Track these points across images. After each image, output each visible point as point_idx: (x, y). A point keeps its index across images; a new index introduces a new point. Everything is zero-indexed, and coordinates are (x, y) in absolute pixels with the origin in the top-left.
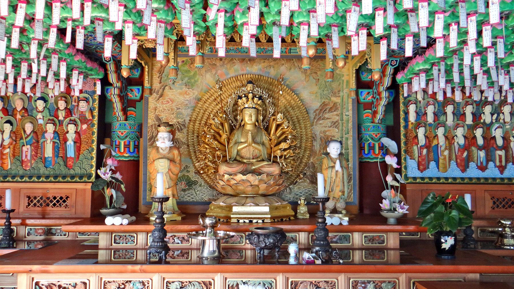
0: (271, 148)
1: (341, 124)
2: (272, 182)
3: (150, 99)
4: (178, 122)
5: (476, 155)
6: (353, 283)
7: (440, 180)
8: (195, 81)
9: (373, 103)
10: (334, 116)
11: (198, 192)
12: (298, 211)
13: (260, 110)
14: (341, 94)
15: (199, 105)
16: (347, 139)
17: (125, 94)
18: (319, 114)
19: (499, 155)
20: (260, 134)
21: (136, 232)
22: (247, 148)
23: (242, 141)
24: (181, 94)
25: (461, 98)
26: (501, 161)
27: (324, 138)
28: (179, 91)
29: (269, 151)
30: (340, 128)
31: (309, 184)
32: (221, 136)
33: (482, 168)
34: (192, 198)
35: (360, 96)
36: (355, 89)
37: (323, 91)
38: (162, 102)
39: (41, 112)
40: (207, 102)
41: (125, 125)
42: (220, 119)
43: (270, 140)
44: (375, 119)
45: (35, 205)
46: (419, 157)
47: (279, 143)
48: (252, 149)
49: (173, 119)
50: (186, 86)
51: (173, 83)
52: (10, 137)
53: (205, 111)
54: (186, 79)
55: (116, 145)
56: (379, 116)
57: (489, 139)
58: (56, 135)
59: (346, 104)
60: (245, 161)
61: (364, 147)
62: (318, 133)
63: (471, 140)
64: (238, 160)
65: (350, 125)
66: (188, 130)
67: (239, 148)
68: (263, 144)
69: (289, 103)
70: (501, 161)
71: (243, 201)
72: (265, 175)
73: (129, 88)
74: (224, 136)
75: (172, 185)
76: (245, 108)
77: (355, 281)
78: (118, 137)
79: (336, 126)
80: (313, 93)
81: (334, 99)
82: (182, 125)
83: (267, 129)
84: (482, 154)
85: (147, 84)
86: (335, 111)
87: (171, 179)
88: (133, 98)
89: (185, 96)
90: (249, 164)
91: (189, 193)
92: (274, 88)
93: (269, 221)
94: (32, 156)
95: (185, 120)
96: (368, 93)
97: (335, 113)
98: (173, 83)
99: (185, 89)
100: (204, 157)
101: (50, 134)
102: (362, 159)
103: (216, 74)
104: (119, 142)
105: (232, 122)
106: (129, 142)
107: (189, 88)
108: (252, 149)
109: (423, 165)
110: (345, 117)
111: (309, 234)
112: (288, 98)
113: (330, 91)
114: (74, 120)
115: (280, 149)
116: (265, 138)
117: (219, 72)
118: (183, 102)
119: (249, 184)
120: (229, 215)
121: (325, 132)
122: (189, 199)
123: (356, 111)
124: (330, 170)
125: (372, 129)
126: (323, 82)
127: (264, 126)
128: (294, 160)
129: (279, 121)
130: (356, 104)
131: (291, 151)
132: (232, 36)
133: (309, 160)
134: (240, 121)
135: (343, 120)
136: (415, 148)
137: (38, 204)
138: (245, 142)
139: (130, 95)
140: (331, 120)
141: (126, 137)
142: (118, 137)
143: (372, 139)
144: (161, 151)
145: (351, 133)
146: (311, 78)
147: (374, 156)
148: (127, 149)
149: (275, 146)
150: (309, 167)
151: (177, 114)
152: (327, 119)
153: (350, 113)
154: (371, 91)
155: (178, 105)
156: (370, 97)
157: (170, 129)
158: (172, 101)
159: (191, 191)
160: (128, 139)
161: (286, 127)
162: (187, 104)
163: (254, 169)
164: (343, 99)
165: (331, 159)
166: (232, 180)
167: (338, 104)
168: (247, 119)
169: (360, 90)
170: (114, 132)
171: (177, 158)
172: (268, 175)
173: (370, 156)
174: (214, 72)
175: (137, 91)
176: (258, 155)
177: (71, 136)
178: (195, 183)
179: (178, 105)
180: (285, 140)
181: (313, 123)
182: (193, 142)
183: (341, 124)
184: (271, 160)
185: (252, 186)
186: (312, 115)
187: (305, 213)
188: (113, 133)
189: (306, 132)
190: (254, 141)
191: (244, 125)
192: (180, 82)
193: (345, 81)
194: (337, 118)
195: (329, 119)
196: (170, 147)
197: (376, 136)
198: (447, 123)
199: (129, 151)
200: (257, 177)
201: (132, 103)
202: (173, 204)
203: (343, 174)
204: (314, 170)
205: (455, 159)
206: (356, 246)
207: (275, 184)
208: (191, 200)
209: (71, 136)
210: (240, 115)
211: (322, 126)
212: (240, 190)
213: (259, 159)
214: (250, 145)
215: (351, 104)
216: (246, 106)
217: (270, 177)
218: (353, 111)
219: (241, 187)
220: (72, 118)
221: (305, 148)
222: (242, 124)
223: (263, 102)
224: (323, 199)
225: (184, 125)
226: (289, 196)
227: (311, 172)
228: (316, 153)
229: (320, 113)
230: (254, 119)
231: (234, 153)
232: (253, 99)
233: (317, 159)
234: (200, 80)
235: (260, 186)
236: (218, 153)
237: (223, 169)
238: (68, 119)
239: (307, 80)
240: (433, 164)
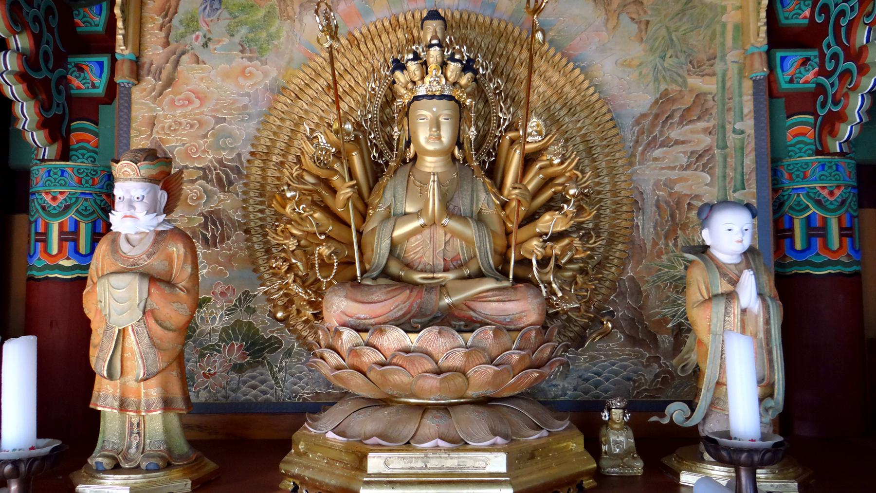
0: (508, 234)
1: (719, 158)
2: (516, 357)
3: (137, 94)
4: (220, 162)
8: (271, 37)
9: (821, 89)
10: (697, 135)
11: (282, 374)
12: (604, 448)
13: (469, 109)
14: (718, 67)
15: (279, 106)
17: (54, 77)
18: (650, 132)
20: (467, 187)
22: (427, 232)
23: (409, 209)
24: (226, 75)
27: (667, 203)
28: (224, 66)
29: (501, 242)
30: (718, 171)
31: (623, 345)
32: (334, 192)
34: (264, 393)
35: (779, 70)
36: (766, 48)
37: (663, 58)
38: (173, 101)
40: (305, 97)
41: (63, 172)
42: (333, 137)
43: (504, 205)
44: (829, 140)
47: (531, 218)
48: (440, 236)
49: (205, 151)
50: (242, 52)
51: (205, 45)
53: (296, 125)
54: (243, 31)
55: (37, 233)
56: (846, 131)
59: (736, 99)
60: (417, 277)
61: (791, 229)
62: (647, 188)
64: (394, 276)
65: (749, 161)
66: (245, 185)
67: (398, 233)
68: (480, 219)
69: (560, 93)
71: (409, 430)
72: (489, 331)
73: (73, 60)
74: (345, 192)
75: (161, 365)
76: (417, 98)
78: (43, 208)
80: (630, 66)
82: (231, 168)
83: (494, 173)
85: (122, 50)
86: (699, 119)
87: (154, 345)
88: (87, 91)
89: (241, 80)
90: (430, 288)
91: (253, 378)
92: (510, 46)
95: (239, 155)
96: (805, 62)
97: (701, 125)
98: (205, 45)
99: (240, 61)
100: (285, 267)
102: (784, 266)
104: (825, 220)
105: (381, 155)
106: (77, 224)
107: (250, 59)
108: (440, 236)
112: (555, 77)
115: (540, 235)
116: (486, 201)
118: (234, 102)
119: (430, 365)
120: (354, 486)
121: (669, 184)
122: (255, 396)
123: (765, 119)
124: (719, 307)
125: (818, 174)
126: (664, 32)
127: (479, 158)
128: (583, 271)
129: (533, 142)
130: (765, 96)
131: (577, 243)
132: (421, 59)
133: (620, 274)
134: (402, 145)
135: (725, 147)
138: (418, 215)
139: (76, 82)
140: (688, 148)
141: (67, 208)
142: (43, 208)
143: (819, 203)
144: (125, 247)
146: (625, 18)
147: (825, 257)
148: (68, 245)
149: (520, 226)
150: (622, 294)
151: (218, 136)
152: (677, 142)
153: (748, 125)
154: (813, 53)
155: (217, 111)
156: (810, 75)
157: (154, 172)
158: (202, 98)
159: (260, 369)
160: (72, 214)
161: (557, 161)
162: (245, 107)
163: (450, 307)
164: (724, 81)
165: (720, 267)
166: (368, 351)
167: (710, 97)
168: (423, 136)
169: (779, 54)
170: (34, 194)
171: (182, 274)
172: (504, 327)
173: (811, 257)
175: (95, 68)
176: (463, 256)
178: (273, 345)
179: (217, 111)
180: (551, 206)
181: (633, 155)
182: (261, 219)
183: (719, 158)
184: (508, 276)
185: (439, 372)
186: (629, 136)
187: (627, 453)
188: (31, 198)
189: (615, 184)
190: (448, 207)
191: (415, 158)
192: (226, 41)
193: (730, 28)
194: (707, 141)
195: (683, 143)
196: (159, 234)
197: (831, 193)
199: (76, 251)
200: (460, 339)
201: (88, 108)
202: (167, 431)
203: (767, 322)
204: (637, 301)
207: (527, 362)
208: (262, 398)
210: (400, 123)
211: (659, 164)
212: (396, 386)
213: (467, 272)
214: (433, 223)
215: (750, 98)
216: (422, 91)
217: (506, 338)
218: (757, 119)
219: (399, 378)
221: (612, 234)
222: (410, 154)
223: (475, 80)
225: (237, 170)
226: (561, 383)
227: (629, 308)
228: (642, 248)
229: (653, 125)
230: (446, 135)
231: (380, 250)
232: (443, 65)
233: (648, 268)
234: (284, 34)
235: (470, 372)
236: (324, 250)
237: (339, 306)
239: (611, 24)
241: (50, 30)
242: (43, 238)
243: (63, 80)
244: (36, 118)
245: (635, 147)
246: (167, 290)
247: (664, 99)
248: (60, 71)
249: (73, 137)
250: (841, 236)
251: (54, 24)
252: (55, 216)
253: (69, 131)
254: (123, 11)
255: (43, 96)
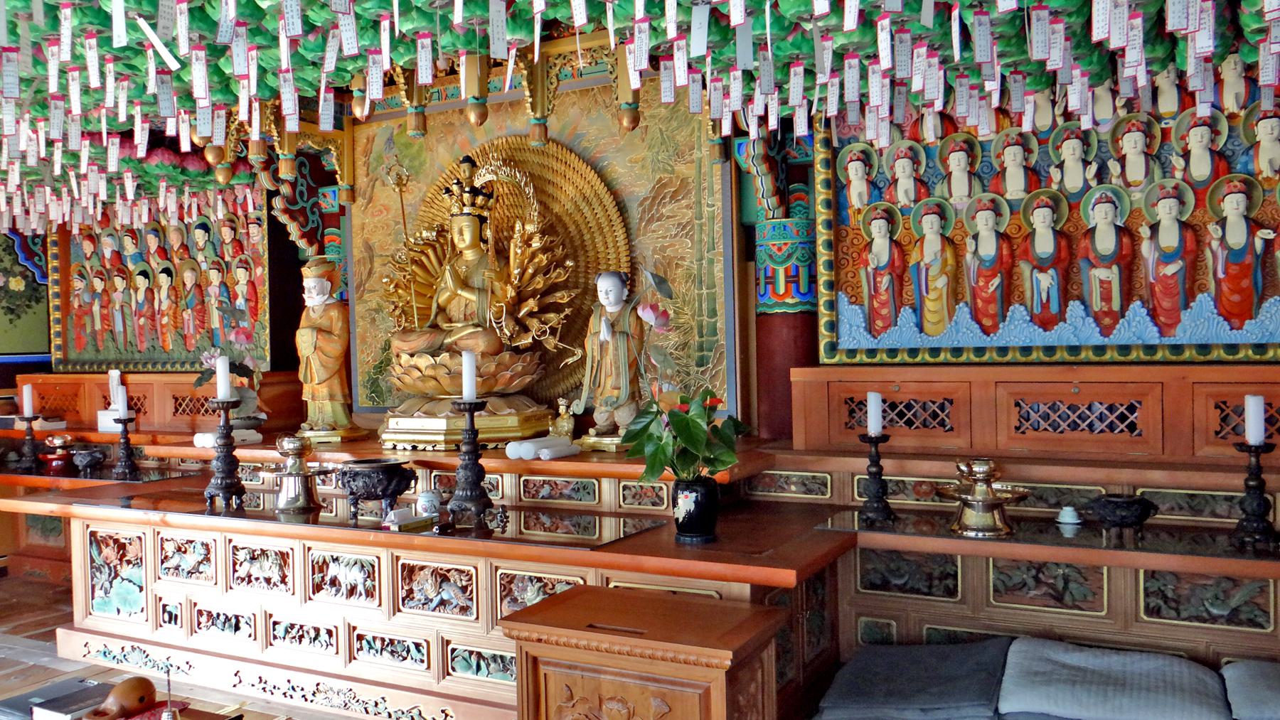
5: (1027, 285)
6: (501, 579)
7: (1155, 354)
8: (421, 164)
10: (679, 210)
14: (697, 154)
16: (711, 262)
17: (308, 205)
18: (650, 211)
19: (1102, 282)
21: (598, 477)
25: (994, 128)
26: (1106, 297)
33: (1107, 321)
39: (202, 250)
45: (184, 411)
46: (871, 297)
52: (169, 297)
57: (1072, 241)
58: (223, 289)
63: (1014, 245)
70: (1106, 297)
77: (508, 576)
78: (771, 256)
79: (687, 234)
81: (682, 169)
84: (1047, 281)
93: (441, 447)
94: (195, 326)
101: (214, 290)
103: (455, 142)
106: (797, 267)
109: (883, 318)
110: (706, 209)
111: (520, 477)
113: (671, 150)
114: (246, 262)
117: (459, 138)
121: (663, 249)
125: (771, 233)
136: (862, 273)
137: (1099, 426)
141: (790, 256)
142: (771, 256)
145: (720, 248)
147: (774, 300)
152: (668, 217)
160: (793, 261)
174: (451, 141)
177: (242, 289)
188: (758, 249)
197: (780, 249)
198: (951, 201)
205: (968, 298)
206: (605, 509)
209: (242, 289)
220: (243, 257)
224: (470, 404)
229: (652, 205)
238: (237, 259)
240: (906, 314)
241: (303, 176)
242: (771, 280)
243: (316, 204)
244: (771, 187)
245: (640, 223)
246: (327, 336)
247: (661, 185)
248: (313, 200)
249: (326, 240)
250: (787, 282)
251: (306, 171)
252: (781, 263)
253: (323, 235)
254: (338, 160)
255: (301, 219)
